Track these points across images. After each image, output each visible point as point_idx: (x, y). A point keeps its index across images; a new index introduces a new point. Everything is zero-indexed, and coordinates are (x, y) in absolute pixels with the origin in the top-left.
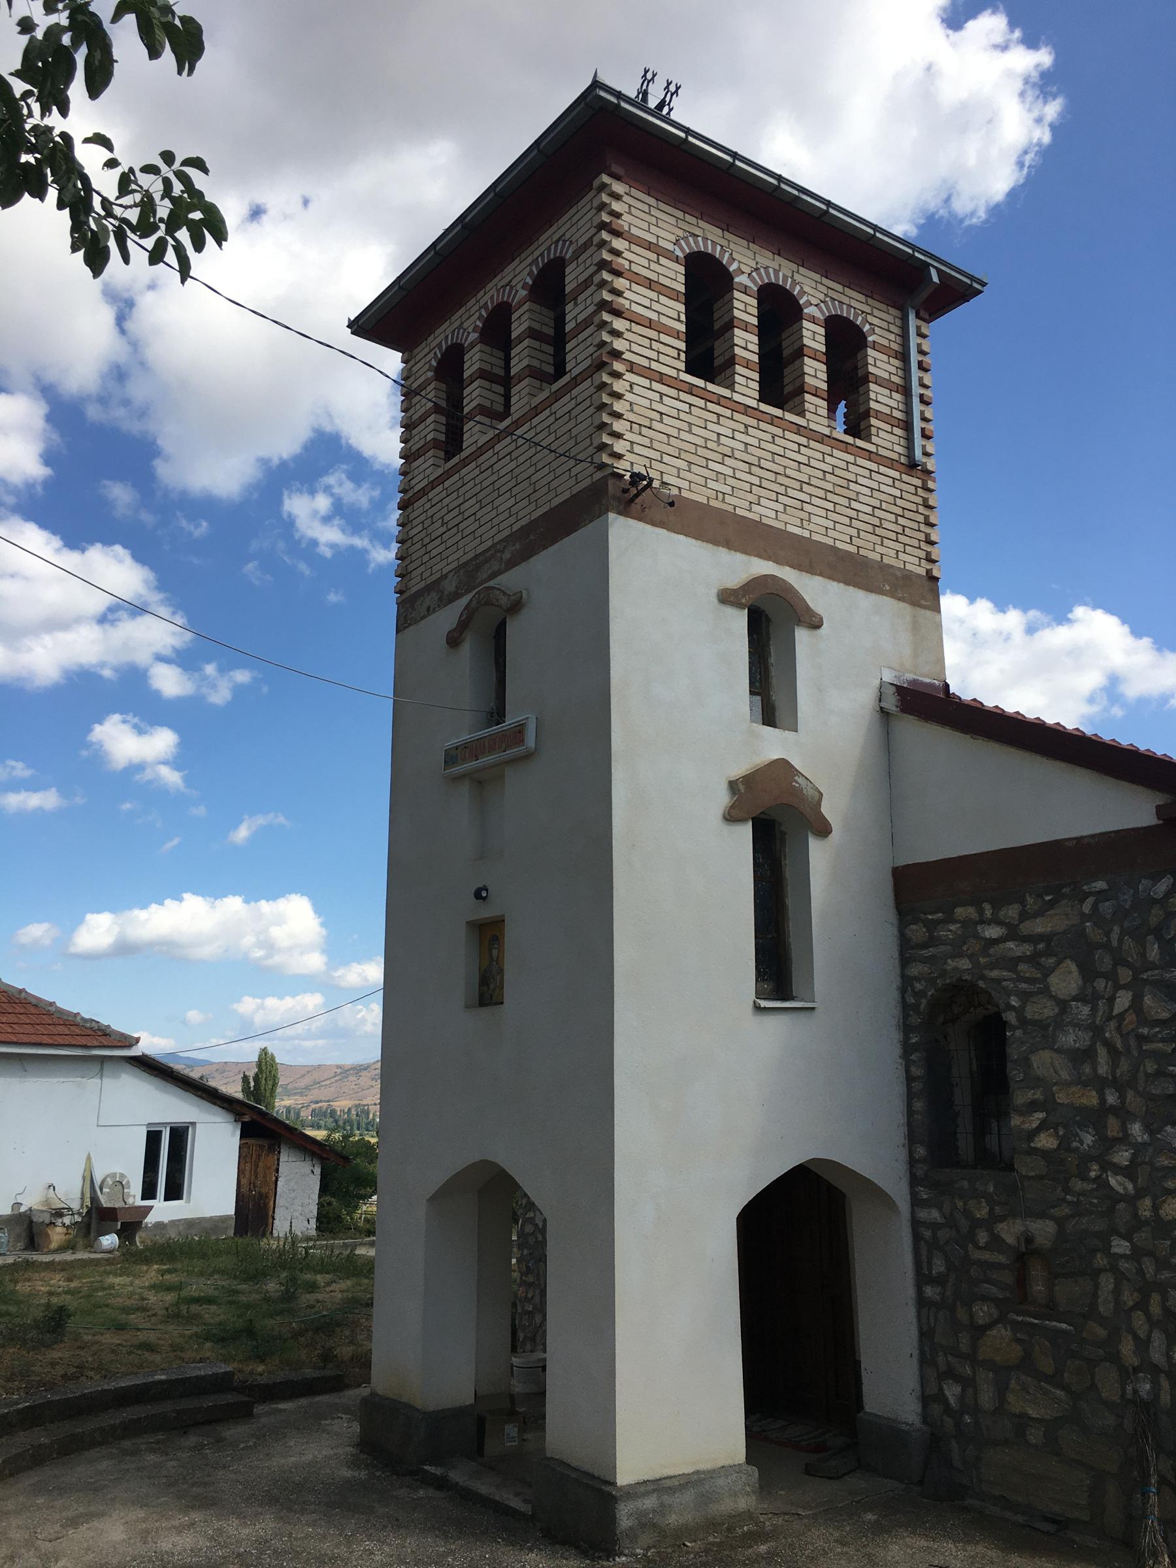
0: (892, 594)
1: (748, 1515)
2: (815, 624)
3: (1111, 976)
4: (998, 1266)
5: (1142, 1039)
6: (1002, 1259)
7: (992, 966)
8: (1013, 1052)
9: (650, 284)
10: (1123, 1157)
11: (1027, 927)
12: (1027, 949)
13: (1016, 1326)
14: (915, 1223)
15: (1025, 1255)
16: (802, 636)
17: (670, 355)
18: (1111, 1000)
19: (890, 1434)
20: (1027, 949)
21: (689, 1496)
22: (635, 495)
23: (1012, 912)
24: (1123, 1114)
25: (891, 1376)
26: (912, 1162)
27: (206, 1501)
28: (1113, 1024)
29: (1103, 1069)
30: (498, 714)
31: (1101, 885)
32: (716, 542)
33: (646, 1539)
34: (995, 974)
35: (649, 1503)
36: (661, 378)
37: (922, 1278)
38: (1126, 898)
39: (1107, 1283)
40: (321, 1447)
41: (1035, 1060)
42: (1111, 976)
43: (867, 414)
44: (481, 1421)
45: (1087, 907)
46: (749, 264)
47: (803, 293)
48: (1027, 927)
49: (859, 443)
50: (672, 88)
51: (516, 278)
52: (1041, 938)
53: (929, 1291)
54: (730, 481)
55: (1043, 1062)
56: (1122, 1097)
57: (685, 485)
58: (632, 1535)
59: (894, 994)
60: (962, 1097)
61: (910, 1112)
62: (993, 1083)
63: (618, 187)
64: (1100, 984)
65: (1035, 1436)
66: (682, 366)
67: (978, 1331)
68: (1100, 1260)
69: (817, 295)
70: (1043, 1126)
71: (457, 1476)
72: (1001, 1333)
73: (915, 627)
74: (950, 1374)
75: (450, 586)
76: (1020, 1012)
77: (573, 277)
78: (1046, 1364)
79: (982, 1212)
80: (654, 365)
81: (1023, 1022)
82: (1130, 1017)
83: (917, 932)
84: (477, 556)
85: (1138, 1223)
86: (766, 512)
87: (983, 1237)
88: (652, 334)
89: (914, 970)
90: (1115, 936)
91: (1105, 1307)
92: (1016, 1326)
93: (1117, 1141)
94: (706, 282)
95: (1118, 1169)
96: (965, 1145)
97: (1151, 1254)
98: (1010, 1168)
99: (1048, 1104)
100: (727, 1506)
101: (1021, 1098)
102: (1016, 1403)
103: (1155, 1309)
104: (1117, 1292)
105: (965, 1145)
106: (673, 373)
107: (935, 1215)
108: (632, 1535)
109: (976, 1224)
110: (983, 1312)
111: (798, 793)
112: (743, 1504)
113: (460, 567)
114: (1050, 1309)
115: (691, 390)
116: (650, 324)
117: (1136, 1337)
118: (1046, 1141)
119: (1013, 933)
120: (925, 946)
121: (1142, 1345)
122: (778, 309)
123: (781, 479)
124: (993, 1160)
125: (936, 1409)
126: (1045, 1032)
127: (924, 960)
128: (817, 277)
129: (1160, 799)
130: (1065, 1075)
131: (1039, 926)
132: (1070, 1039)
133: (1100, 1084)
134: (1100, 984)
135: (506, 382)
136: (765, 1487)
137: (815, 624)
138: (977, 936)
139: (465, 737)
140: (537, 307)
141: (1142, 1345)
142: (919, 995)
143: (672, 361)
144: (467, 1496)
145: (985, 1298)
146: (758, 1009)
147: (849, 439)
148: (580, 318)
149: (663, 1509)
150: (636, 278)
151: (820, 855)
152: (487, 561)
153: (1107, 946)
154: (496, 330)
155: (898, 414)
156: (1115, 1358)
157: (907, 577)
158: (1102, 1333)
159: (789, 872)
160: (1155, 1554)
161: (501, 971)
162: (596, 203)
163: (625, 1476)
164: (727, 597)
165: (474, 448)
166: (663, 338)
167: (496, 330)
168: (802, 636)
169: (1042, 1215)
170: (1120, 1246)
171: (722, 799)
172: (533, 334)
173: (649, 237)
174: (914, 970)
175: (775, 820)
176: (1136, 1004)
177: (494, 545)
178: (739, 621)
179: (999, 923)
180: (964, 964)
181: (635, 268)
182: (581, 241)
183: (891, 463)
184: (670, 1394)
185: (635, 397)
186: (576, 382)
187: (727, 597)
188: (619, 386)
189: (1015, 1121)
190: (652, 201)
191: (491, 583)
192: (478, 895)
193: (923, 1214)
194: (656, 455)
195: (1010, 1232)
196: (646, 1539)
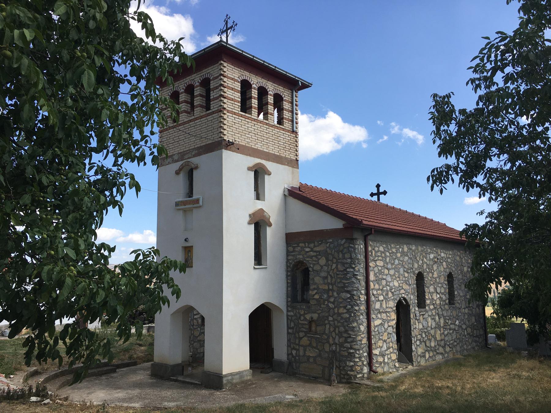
0: (287, 165)
1: (250, 380)
2: (269, 174)
3: (332, 261)
4: (305, 324)
5: (338, 274)
6: (306, 323)
7: (307, 257)
8: (311, 277)
9: (232, 89)
10: (332, 300)
11: (315, 249)
12: (315, 254)
13: (308, 337)
14: (287, 316)
15: (311, 322)
16: (266, 177)
17: (237, 107)
18: (332, 266)
19: (281, 363)
20: (315, 254)
21: (237, 376)
22: (229, 145)
23: (312, 245)
24: (332, 290)
25: (280, 350)
26: (287, 302)
27: (119, 388)
28: (332, 271)
29: (329, 281)
30: (190, 193)
31: (331, 240)
32: (247, 155)
33: (229, 385)
34: (308, 259)
35: (230, 378)
36: (235, 113)
37: (289, 328)
38: (336, 244)
39: (328, 326)
40: (141, 375)
41: (315, 279)
42: (332, 261)
43: (283, 118)
44: (183, 367)
45: (328, 245)
46: (256, 81)
47: (268, 88)
48: (315, 249)
49: (281, 126)
50: (235, 24)
51: (196, 79)
52: (319, 252)
53: (290, 331)
54: (251, 139)
55: (317, 279)
56: (333, 287)
57: (240, 141)
58: (226, 384)
59: (285, 263)
60: (299, 287)
61: (287, 291)
62: (306, 284)
63: (225, 64)
64: (330, 262)
65: (311, 360)
66: (240, 110)
67: (300, 338)
68: (326, 322)
69: (272, 88)
70: (316, 293)
71: (180, 378)
72: (305, 338)
73: (293, 173)
74: (294, 349)
75: (176, 158)
76: (313, 268)
77: (213, 85)
78: (315, 345)
79: (302, 313)
80: (233, 110)
81: (313, 270)
82: (335, 270)
83: (291, 249)
84: (184, 152)
85: (334, 314)
86: (259, 146)
87: (302, 318)
88: (233, 102)
89: (290, 258)
90: (333, 252)
91: (327, 332)
92: (308, 337)
93: (331, 296)
94: (246, 86)
95: (331, 302)
96: (299, 298)
97: (336, 320)
98: (309, 303)
99: (318, 289)
100: (246, 378)
101: (312, 287)
102: (308, 353)
103: (337, 331)
104: (329, 329)
105: (299, 298)
106: (237, 112)
107: (292, 314)
108: (226, 384)
109: (301, 315)
110: (301, 334)
111: (264, 216)
112: (249, 378)
113: (179, 153)
114: (316, 333)
115: (242, 116)
116: (232, 100)
117: (333, 337)
118: (317, 297)
119: (312, 250)
120: (292, 252)
121: (334, 339)
122: (263, 92)
123: (262, 137)
124: (305, 301)
125: (290, 356)
126: (317, 272)
127: (293, 256)
128: (272, 83)
129: (344, 222)
130: (321, 282)
131: (317, 249)
132: (323, 274)
133: (328, 284)
134: (330, 262)
135: (193, 107)
136: (253, 375)
137: (269, 174)
138: (304, 250)
139: (181, 199)
140: (202, 88)
141: (334, 339)
142: (290, 263)
143: (237, 109)
144: (184, 382)
145: (302, 331)
146: (254, 268)
147: (278, 126)
148: (215, 96)
149: (232, 379)
150: (229, 88)
151: (269, 231)
152: (187, 153)
153: (331, 254)
154: (190, 90)
155: (290, 118)
156: (328, 342)
157: (291, 160)
158: (326, 337)
159: (262, 235)
160: (334, 381)
161: (192, 259)
162: (219, 68)
163: (224, 373)
164: (249, 169)
165: (183, 122)
166: (236, 103)
167: (190, 90)
168: (266, 177)
169: (315, 313)
170: (331, 319)
171: (248, 219)
172: (201, 95)
173: (232, 75)
174: (290, 258)
175: (259, 223)
176: (337, 267)
177: (189, 150)
178: (252, 174)
179: (309, 248)
180: (301, 257)
181: (229, 85)
182: (215, 76)
183: (288, 131)
184: (234, 354)
185: (229, 119)
186: (213, 113)
187: (249, 169)
188: (225, 117)
189: (310, 292)
190: (233, 67)
191: (188, 160)
192: (186, 240)
193: (289, 314)
194: (233, 134)
195: (308, 317)
196: (229, 385)
